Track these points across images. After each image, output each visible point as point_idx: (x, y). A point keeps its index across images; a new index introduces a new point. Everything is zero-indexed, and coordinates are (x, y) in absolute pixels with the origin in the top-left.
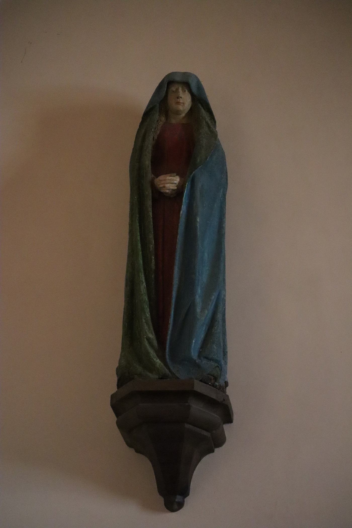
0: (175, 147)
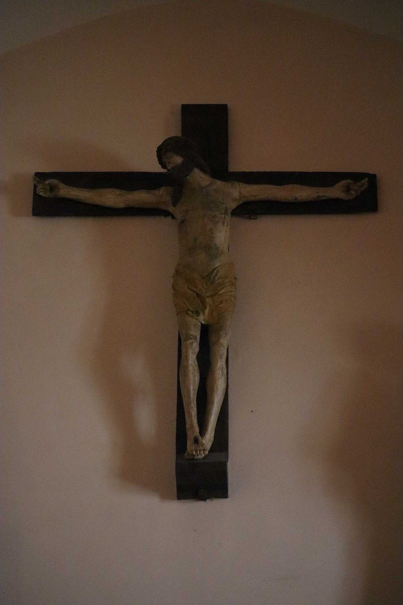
0: (357, 196)
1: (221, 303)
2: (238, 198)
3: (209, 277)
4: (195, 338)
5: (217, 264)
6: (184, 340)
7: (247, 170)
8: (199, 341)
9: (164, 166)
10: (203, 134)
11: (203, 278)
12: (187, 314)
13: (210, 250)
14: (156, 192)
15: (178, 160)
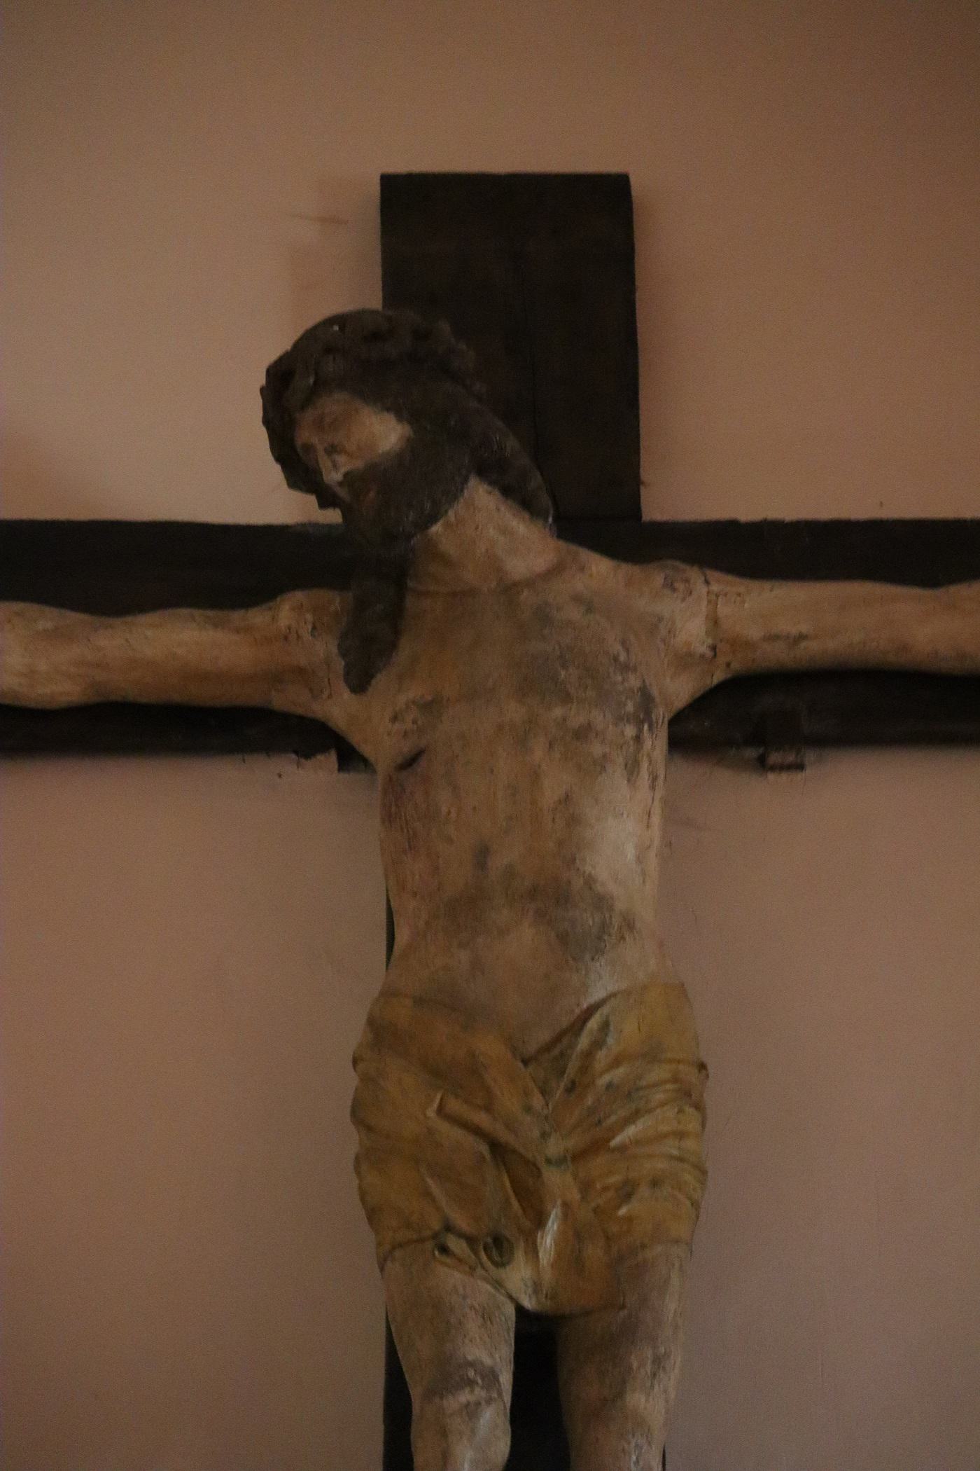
1: (627, 1192)
2: (703, 649)
3: (558, 1058)
4: (491, 1377)
5: (602, 982)
6: (430, 1394)
7: (747, 512)
8: (507, 1398)
9: (297, 467)
10: (499, 322)
11: (526, 1062)
12: (444, 1250)
13: (560, 902)
14: (257, 617)
15: (384, 433)
